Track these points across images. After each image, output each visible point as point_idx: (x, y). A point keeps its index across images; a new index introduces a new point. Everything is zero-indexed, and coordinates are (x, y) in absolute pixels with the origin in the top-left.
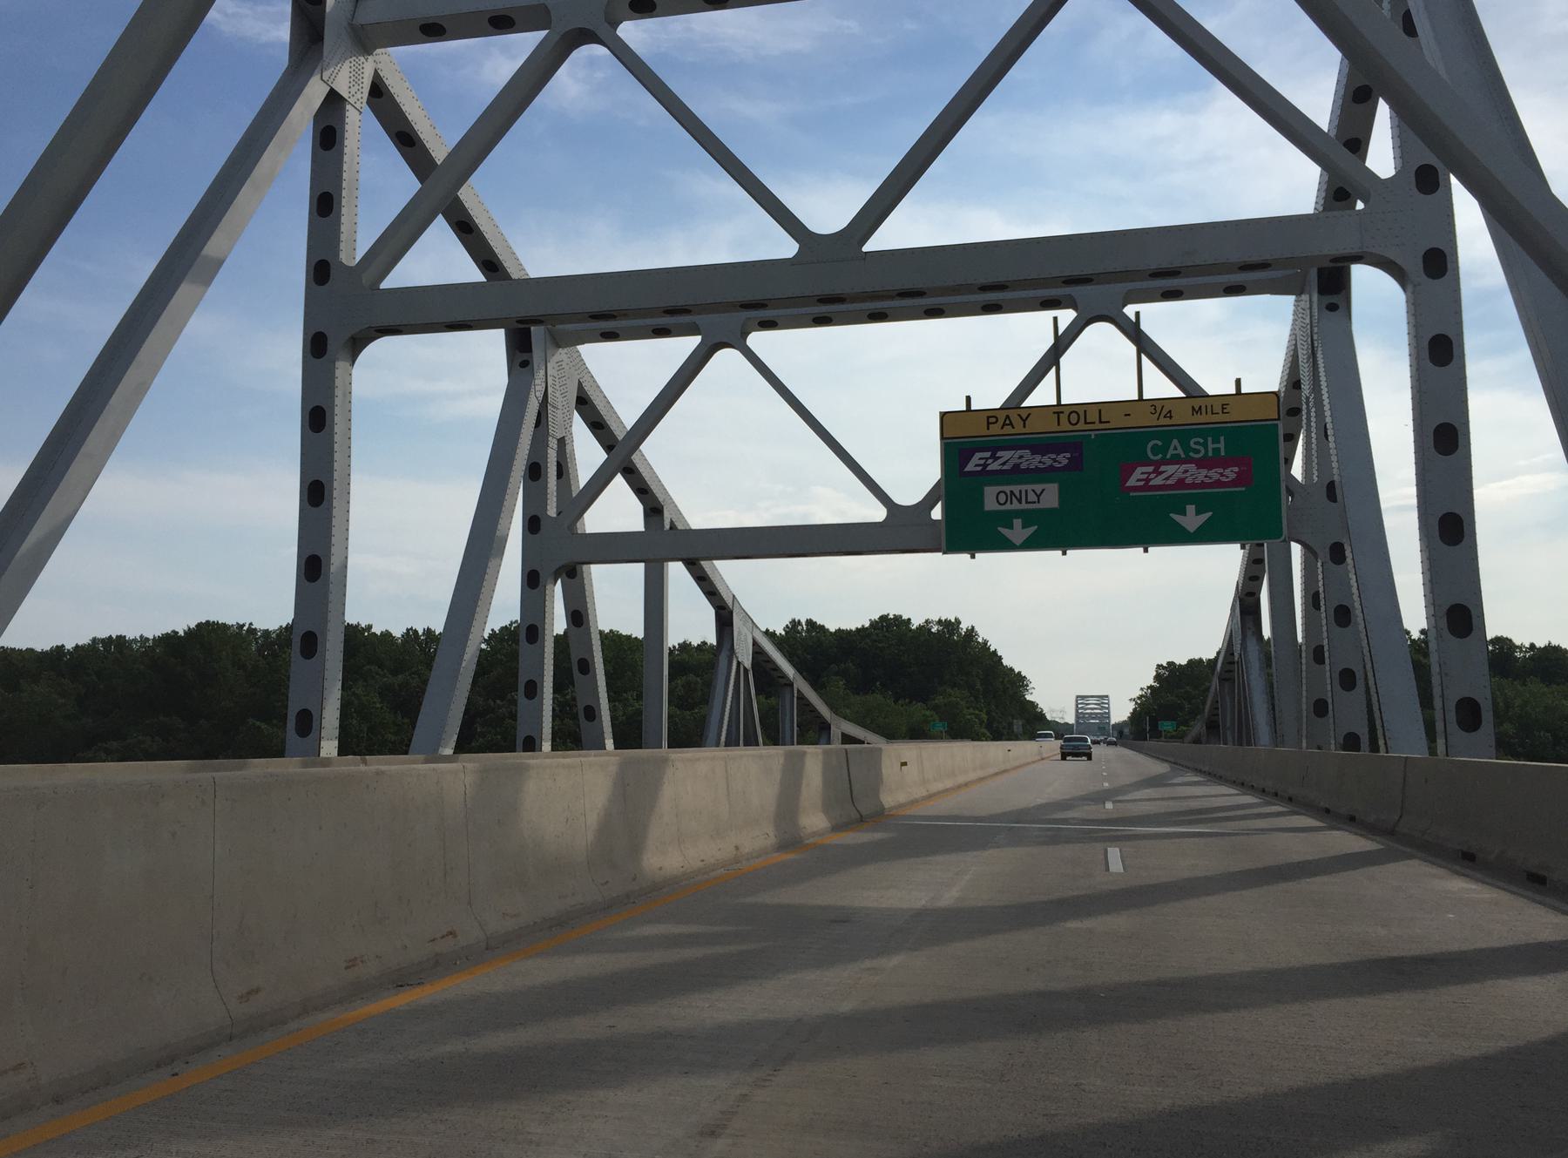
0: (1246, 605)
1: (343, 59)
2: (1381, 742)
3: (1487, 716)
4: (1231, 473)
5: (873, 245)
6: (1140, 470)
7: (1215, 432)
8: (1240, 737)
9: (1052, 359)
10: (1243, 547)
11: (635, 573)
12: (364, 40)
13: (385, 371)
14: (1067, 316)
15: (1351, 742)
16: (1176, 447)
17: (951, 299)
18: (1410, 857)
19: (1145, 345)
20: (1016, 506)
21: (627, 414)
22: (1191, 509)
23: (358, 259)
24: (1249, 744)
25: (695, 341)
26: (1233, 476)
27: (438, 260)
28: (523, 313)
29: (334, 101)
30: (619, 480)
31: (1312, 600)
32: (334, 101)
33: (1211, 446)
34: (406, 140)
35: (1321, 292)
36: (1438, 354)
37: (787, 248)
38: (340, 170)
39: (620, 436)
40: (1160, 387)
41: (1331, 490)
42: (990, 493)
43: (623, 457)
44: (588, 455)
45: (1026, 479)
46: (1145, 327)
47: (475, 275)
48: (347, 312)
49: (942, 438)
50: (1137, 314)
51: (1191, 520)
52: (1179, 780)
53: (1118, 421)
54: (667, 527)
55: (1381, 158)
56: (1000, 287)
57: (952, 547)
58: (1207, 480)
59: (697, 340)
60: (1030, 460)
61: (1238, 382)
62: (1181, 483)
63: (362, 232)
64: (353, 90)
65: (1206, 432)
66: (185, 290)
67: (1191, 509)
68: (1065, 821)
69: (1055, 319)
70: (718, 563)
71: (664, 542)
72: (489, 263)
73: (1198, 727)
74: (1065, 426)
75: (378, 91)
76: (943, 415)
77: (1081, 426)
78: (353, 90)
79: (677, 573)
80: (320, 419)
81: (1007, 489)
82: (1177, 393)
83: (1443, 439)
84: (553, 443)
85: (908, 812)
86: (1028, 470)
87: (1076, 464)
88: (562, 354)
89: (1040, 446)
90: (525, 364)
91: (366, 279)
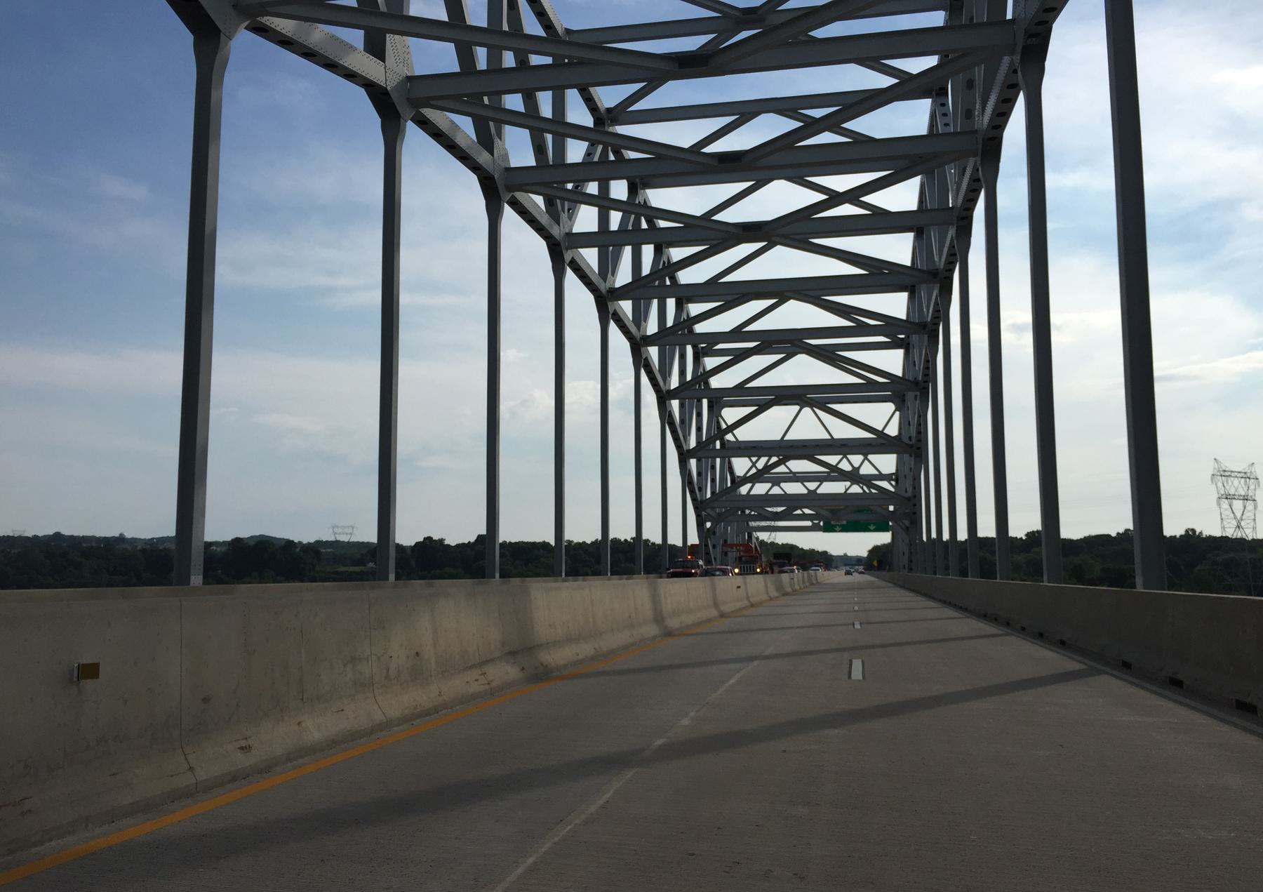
18: (1100, 672)
51: (872, 527)
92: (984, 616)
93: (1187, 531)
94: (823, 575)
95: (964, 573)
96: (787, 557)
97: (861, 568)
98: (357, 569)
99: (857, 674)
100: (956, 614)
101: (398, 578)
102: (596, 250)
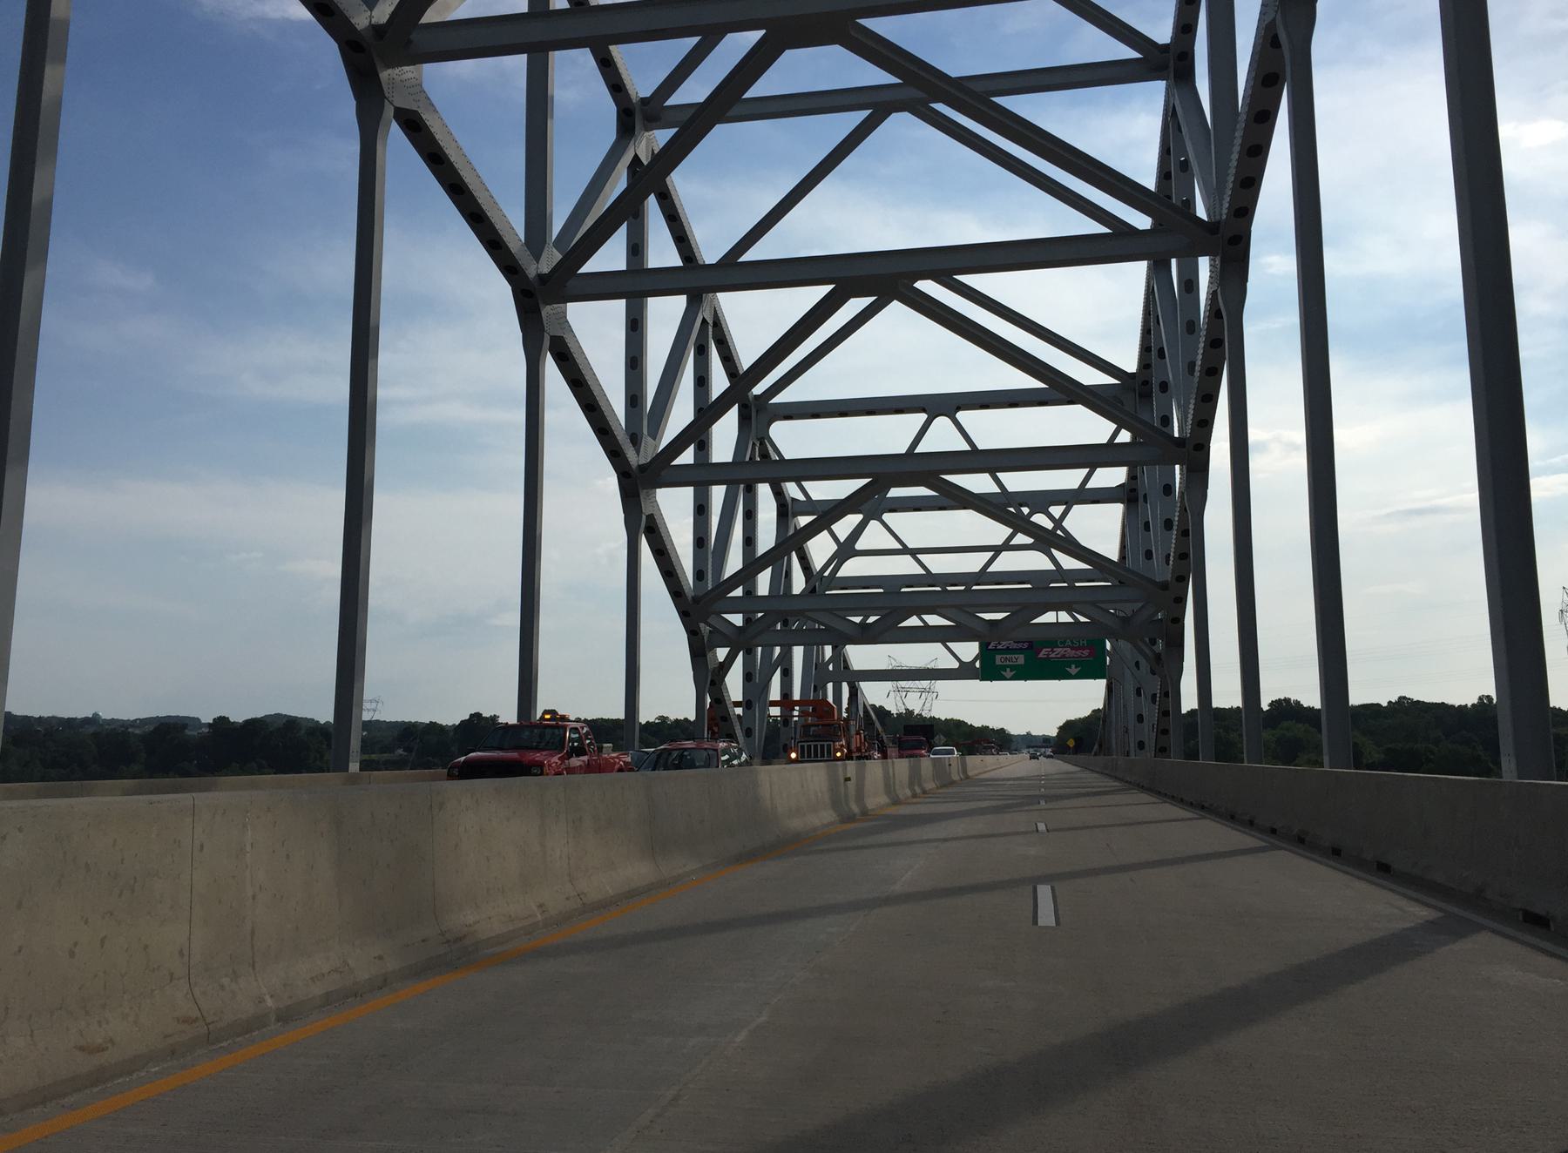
4: (1086, 652)
18: (1480, 928)
42: (998, 657)
51: (1073, 670)
92: (1231, 818)
93: (1480, 698)
94: (982, 764)
95: (1192, 754)
96: (918, 734)
97: (1049, 751)
98: (386, 756)
99: (1046, 917)
100: (1189, 815)
101: (366, 766)
102: (623, 302)
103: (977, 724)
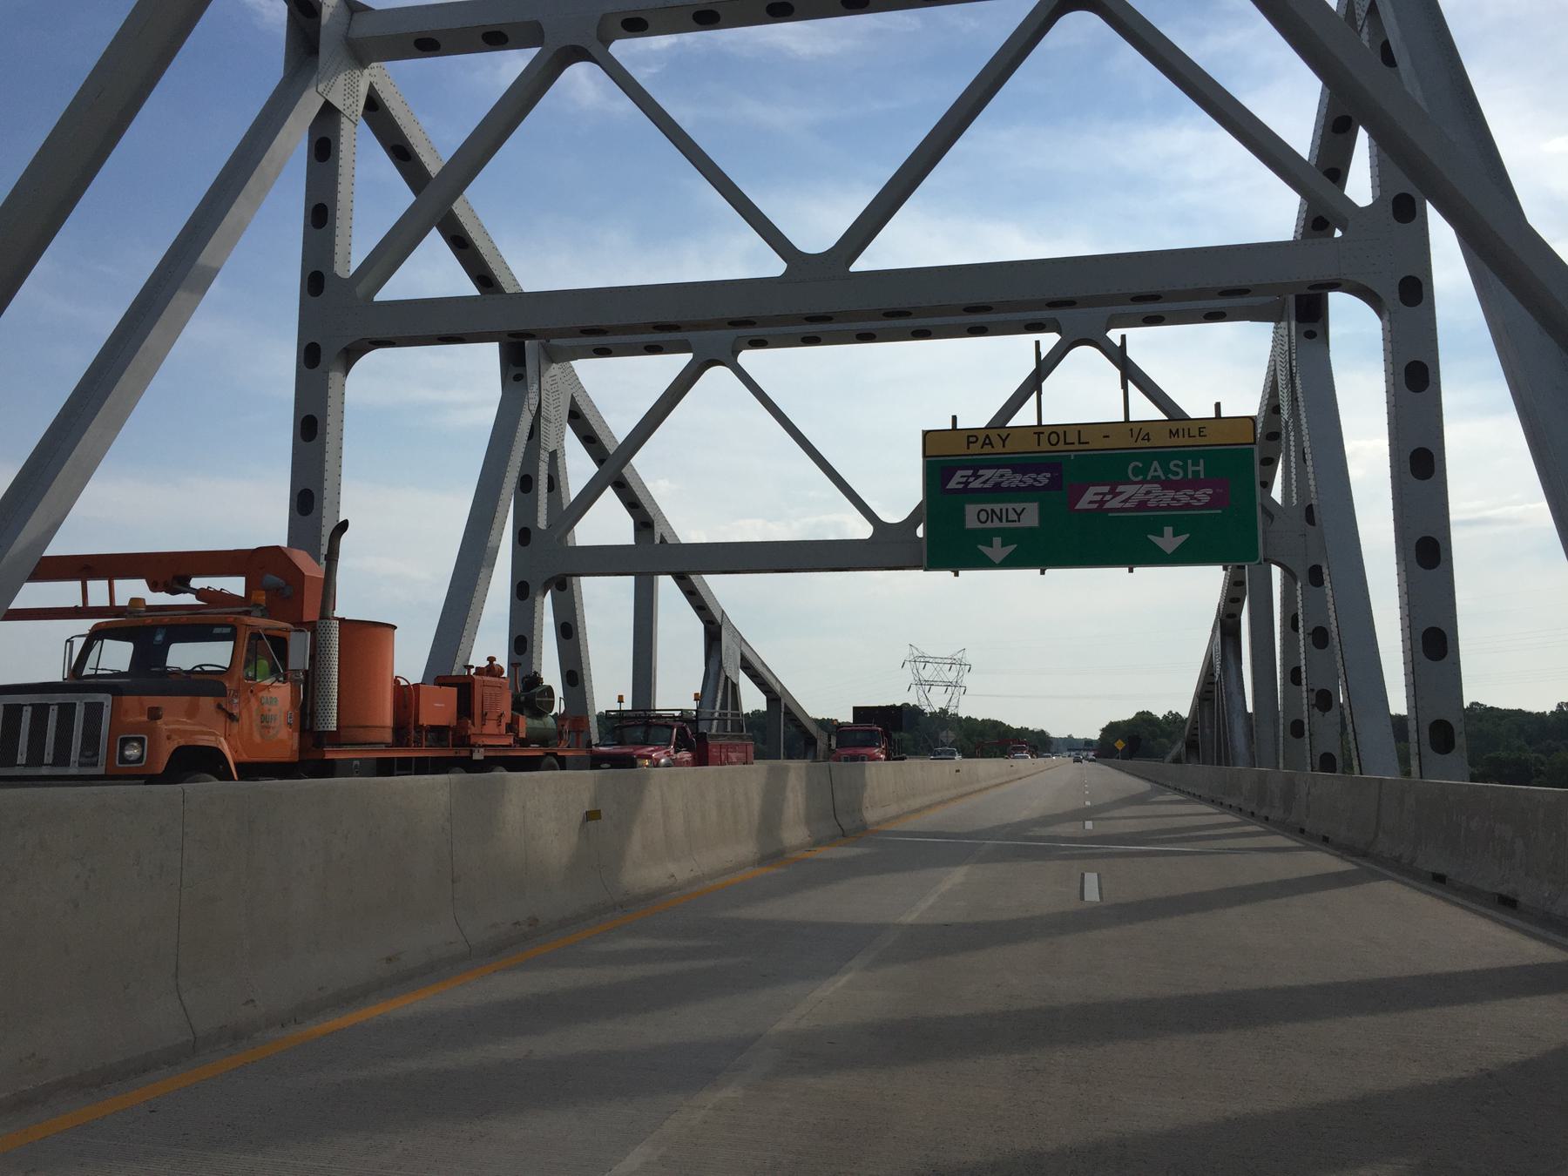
0: (1227, 626)
1: (336, 73)
2: (1355, 763)
3: (1460, 740)
4: (1204, 495)
5: (860, 265)
6: (1092, 490)
7: (1194, 455)
8: (1219, 758)
9: (1034, 384)
10: (1225, 569)
11: (92, 603)
12: (360, 54)
13: (377, 382)
14: (1049, 340)
15: (1327, 762)
16: (1156, 469)
17: (937, 321)
18: (1386, 878)
19: (1130, 373)
20: (996, 524)
21: (619, 425)
22: (1168, 530)
23: (352, 271)
24: (1227, 764)
25: (686, 358)
26: (1207, 499)
27: (432, 273)
28: (515, 327)
29: (329, 113)
30: (609, 494)
31: (1291, 622)
32: (329, 113)
33: (1191, 469)
34: (402, 153)
35: (1298, 320)
36: (1414, 378)
37: (775, 267)
38: (335, 183)
39: (611, 449)
40: (1144, 410)
41: (1309, 514)
42: (971, 510)
43: (614, 470)
44: (579, 467)
45: (1003, 501)
46: (1131, 353)
47: (469, 288)
48: (341, 325)
49: (925, 456)
50: (1123, 337)
51: (1168, 541)
52: (1161, 798)
53: (1097, 443)
54: (657, 541)
55: (1360, 186)
56: (986, 309)
57: (933, 564)
58: (1174, 504)
59: (688, 357)
60: (1011, 479)
61: (1218, 406)
62: (1142, 505)
63: (357, 244)
64: (348, 102)
65: (1185, 455)
66: (181, 297)
67: (1168, 530)
68: (1041, 839)
69: (1037, 343)
70: (708, 578)
71: (653, 556)
72: (484, 277)
73: (1179, 747)
74: (1045, 446)
75: (374, 106)
76: (926, 434)
77: (1061, 446)
78: (348, 102)
79: (666, 586)
80: (312, 428)
81: (988, 507)
82: (1159, 415)
83: (1419, 461)
84: (544, 456)
85: (893, 828)
86: (1009, 489)
87: (1055, 484)
88: (555, 369)
89: (1021, 467)
90: (520, 377)
91: (361, 290)
94: (888, 783)
97: (1091, 755)
100: (1289, 843)
103: (1016, 725)
